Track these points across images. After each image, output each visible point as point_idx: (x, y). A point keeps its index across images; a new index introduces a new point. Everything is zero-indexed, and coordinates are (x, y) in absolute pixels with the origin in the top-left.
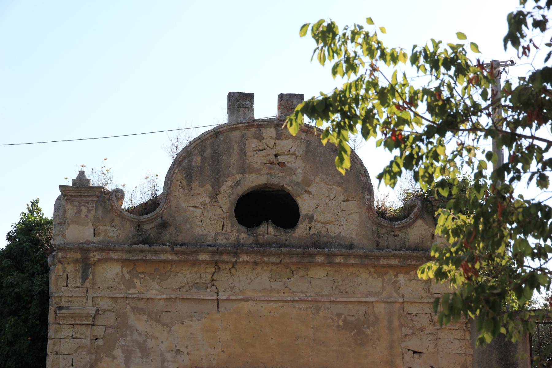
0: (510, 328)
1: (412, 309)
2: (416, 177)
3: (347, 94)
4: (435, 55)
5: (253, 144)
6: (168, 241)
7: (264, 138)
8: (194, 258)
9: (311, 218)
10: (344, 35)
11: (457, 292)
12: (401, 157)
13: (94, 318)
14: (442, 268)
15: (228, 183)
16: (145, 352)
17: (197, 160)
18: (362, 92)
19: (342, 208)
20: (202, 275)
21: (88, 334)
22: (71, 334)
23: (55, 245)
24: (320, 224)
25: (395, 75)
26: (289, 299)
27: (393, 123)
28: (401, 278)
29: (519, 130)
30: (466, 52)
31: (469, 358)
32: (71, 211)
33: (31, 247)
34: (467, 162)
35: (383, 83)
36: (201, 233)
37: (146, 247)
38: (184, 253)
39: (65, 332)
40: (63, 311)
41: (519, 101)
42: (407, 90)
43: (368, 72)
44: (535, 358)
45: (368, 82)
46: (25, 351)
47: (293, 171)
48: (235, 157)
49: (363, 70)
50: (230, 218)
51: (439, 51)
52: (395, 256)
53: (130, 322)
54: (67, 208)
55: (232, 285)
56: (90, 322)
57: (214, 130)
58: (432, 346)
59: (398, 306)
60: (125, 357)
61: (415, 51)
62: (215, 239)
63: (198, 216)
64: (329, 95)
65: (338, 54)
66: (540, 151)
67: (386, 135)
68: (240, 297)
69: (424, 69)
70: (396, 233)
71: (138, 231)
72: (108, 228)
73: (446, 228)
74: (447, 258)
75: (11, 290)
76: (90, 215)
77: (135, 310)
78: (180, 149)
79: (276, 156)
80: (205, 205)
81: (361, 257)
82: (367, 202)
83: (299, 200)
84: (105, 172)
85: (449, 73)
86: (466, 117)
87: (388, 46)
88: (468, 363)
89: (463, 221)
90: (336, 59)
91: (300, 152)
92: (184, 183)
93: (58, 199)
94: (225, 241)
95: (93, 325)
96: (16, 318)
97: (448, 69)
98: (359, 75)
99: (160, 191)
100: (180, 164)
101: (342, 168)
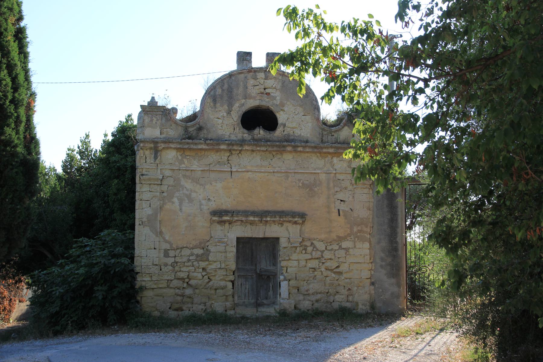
0: (394, 185)
1: (341, 177)
2: (343, 99)
3: (304, 51)
4: (355, 27)
5: (252, 82)
6: (203, 138)
7: (258, 79)
8: (218, 147)
9: (284, 125)
10: (303, 15)
11: (365, 165)
12: (334, 87)
13: (161, 180)
14: (357, 152)
15: (237, 105)
16: (191, 200)
17: (219, 91)
18: (313, 49)
19: (302, 119)
20: (222, 157)
21: (159, 190)
22: (149, 190)
23: (139, 139)
24: (289, 129)
25: (332, 39)
26: (271, 171)
27: (331, 67)
28: (335, 160)
29: (403, 72)
30: (373, 26)
31: (372, 204)
32: (147, 120)
33: (125, 140)
34: (373, 91)
35: (325, 44)
36: (221, 133)
37: (190, 141)
38: (212, 144)
39: (146, 188)
40: (144, 177)
41: (402, 54)
42: (339, 47)
43: (316, 37)
44: (407, 201)
45: (316, 43)
46: (124, 199)
47: (274, 98)
48: (241, 89)
49: (313, 36)
50: (238, 125)
51: (357, 25)
52: (331, 147)
53: (182, 183)
54: (145, 118)
55: (239, 163)
56: (160, 183)
57: (229, 73)
58: (351, 197)
59: (333, 175)
60: (179, 202)
61: (343, 25)
62: (230, 137)
63: (220, 123)
64: (294, 51)
65: (299, 26)
66: (414, 84)
67: (326, 74)
68: (244, 170)
69: (349, 36)
70: (333, 134)
71: (185, 132)
72: (169, 130)
73: (359, 130)
74: (360, 146)
75: (115, 164)
76: (158, 122)
77: (185, 176)
78: (209, 85)
79: (265, 89)
80: (224, 117)
81: (312, 147)
82: (316, 116)
83: (278, 115)
84: (167, 98)
85: (363, 38)
86: (373, 64)
87: (328, 20)
88: (371, 206)
89: (369, 125)
90: (298, 29)
91: (279, 87)
92: (212, 104)
93: (140, 113)
94: (235, 138)
95: (161, 184)
96: (118, 180)
97: (362, 35)
98: (311, 39)
99: (198, 109)
100: (209, 93)
101: (301, 94)
